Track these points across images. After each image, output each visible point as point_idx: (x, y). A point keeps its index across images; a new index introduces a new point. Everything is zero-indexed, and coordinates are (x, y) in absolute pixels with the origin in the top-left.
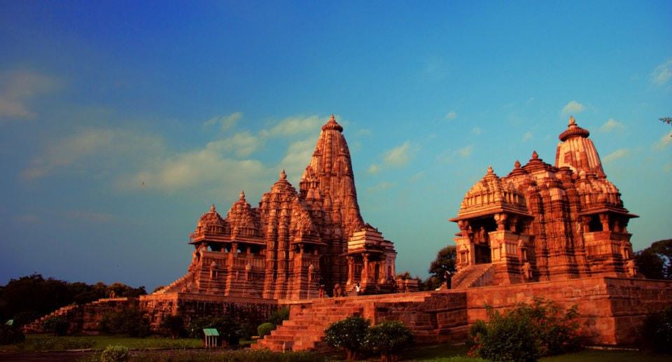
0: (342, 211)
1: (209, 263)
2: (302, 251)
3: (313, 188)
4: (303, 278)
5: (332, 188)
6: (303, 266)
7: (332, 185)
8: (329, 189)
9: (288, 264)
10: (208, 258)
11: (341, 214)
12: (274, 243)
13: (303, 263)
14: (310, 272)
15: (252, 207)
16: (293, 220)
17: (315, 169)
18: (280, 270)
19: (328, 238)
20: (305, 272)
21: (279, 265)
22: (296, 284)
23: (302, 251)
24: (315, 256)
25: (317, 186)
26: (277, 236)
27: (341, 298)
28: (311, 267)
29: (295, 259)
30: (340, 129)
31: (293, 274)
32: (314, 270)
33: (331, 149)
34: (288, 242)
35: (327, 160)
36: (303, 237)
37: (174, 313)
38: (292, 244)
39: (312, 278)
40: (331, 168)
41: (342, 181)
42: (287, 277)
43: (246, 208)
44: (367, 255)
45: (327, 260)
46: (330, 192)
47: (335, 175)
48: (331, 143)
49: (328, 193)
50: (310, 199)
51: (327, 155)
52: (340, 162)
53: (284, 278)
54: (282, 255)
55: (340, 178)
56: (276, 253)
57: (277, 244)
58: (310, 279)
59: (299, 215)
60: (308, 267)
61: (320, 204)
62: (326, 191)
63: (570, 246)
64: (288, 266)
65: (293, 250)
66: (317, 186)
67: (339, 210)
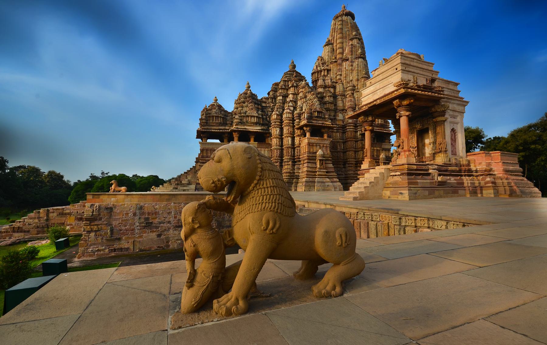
0: (355, 94)
1: (209, 155)
2: (308, 134)
3: (324, 75)
4: (310, 165)
5: (343, 73)
6: (309, 152)
7: (344, 69)
8: (341, 75)
9: (294, 151)
10: (207, 150)
11: (354, 98)
12: (278, 130)
13: (309, 148)
14: (318, 158)
15: (259, 98)
16: (299, 103)
17: (326, 58)
18: (285, 158)
19: (341, 123)
20: (312, 158)
21: (285, 152)
22: (302, 172)
23: (308, 134)
24: (325, 139)
25: (328, 73)
26: (281, 122)
27: (17, 312)
28: (320, 152)
29: (302, 145)
30: (351, 15)
31: (300, 161)
32: (323, 156)
33: (342, 33)
34: (294, 126)
35: (338, 46)
36: (307, 119)
37: (229, 202)
38: (297, 129)
39: (321, 164)
40: (342, 53)
41: (355, 64)
42: (294, 165)
43: (249, 97)
44: (405, 103)
45: (340, 146)
46: (342, 78)
47: (347, 60)
48: (342, 29)
49: (340, 79)
50: (321, 86)
51: (338, 41)
52: (352, 45)
53: (290, 167)
54: (287, 141)
55: (352, 62)
56: (281, 139)
57: (282, 129)
58: (318, 166)
59: (306, 97)
60: (316, 153)
61: (332, 90)
62: (338, 77)
63: (406, 174)
64: (294, 153)
65: (299, 136)
66: (328, 73)
67: (353, 94)
